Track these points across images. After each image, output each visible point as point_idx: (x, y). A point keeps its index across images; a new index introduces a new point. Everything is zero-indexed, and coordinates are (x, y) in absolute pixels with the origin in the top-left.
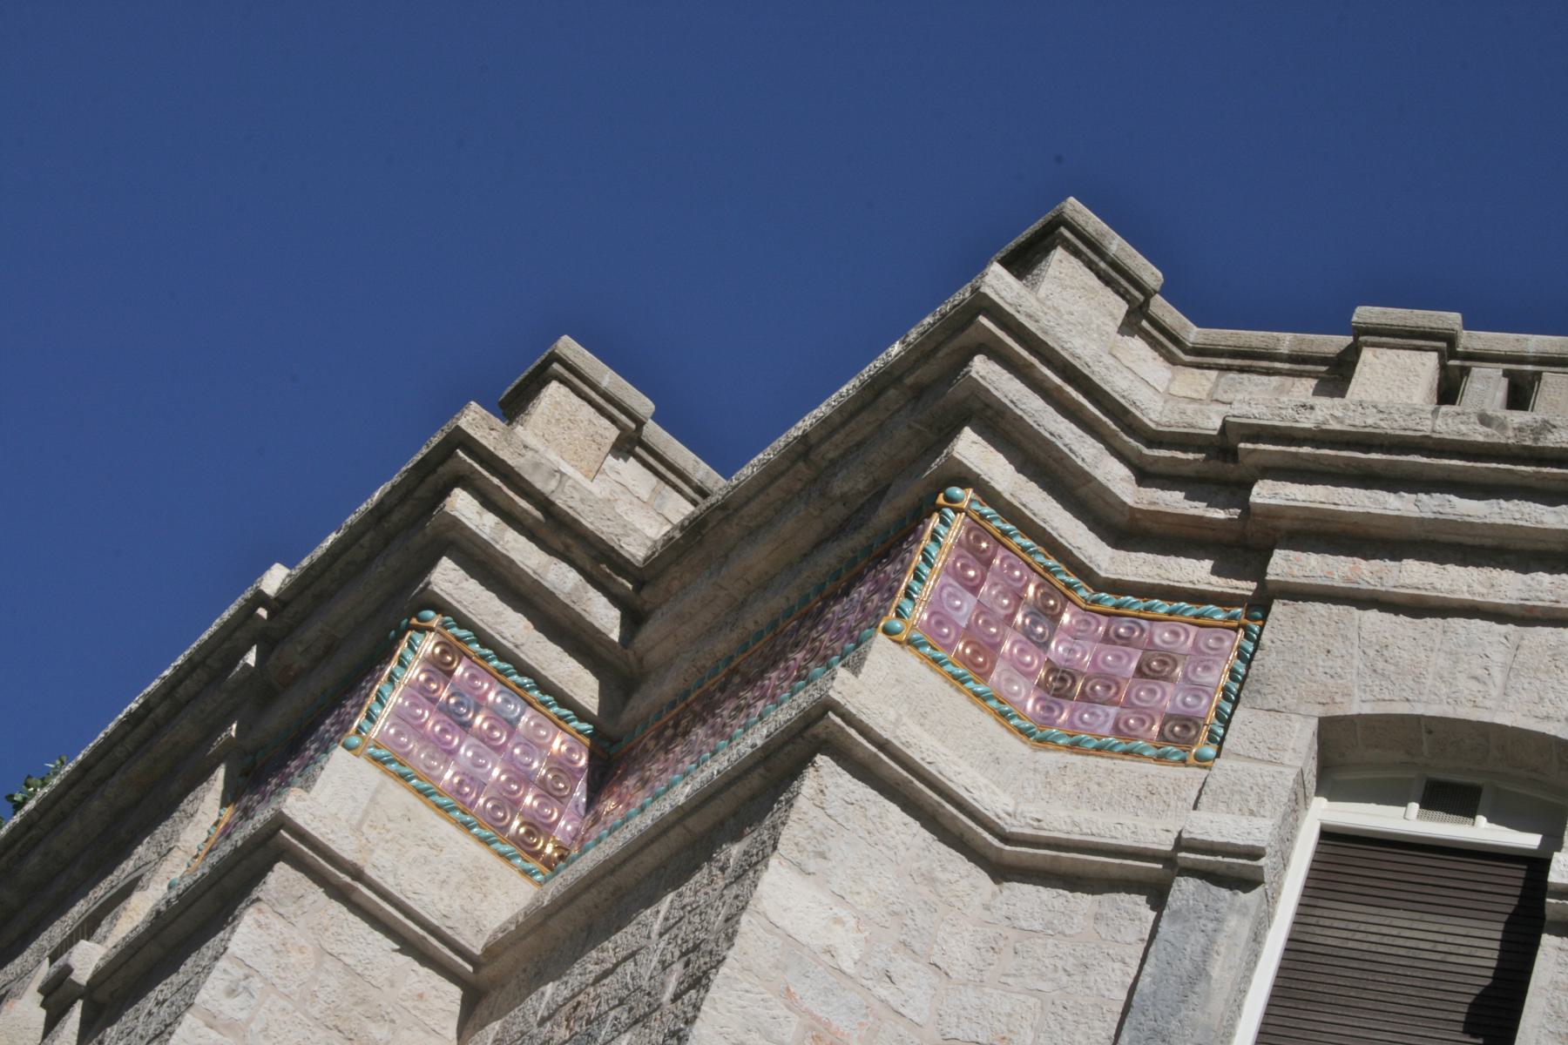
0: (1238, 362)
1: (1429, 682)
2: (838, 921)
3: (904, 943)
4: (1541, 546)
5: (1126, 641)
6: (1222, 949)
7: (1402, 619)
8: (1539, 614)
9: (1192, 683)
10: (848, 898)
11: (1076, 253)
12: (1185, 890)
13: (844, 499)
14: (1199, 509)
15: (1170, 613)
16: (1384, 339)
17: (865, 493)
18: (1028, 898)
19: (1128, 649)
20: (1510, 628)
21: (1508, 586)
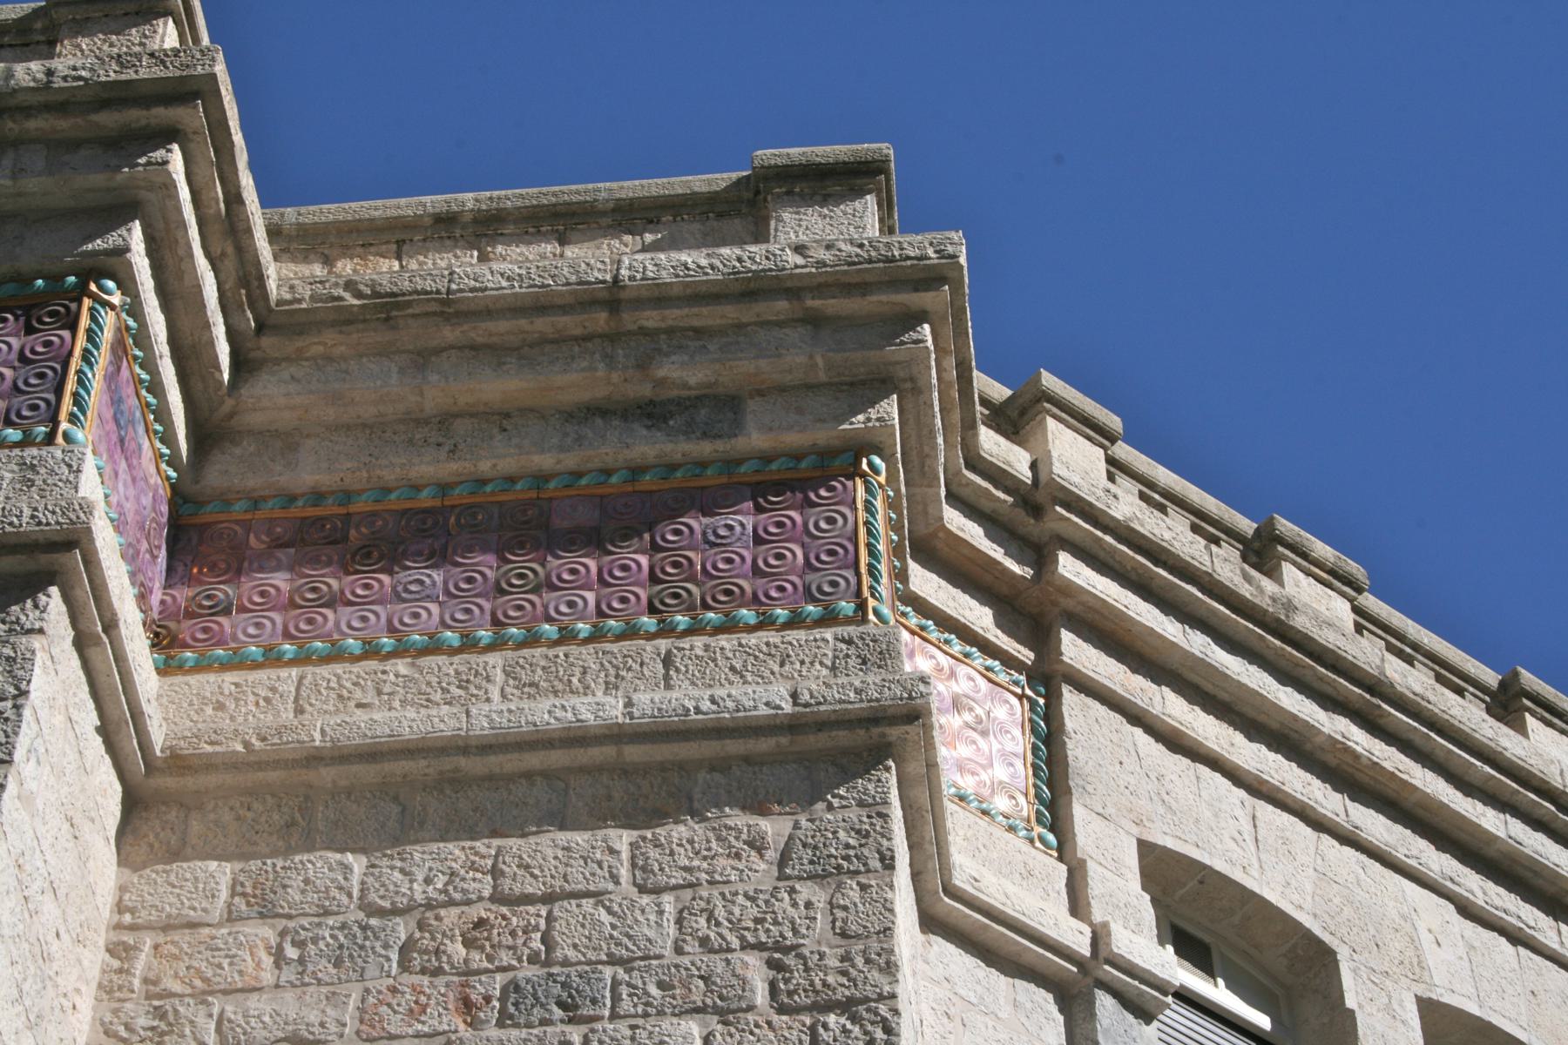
4: (1262, 718)
7: (1160, 747)
8: (1264, 789)
13: (661, 383)
14: (996, 552)
16: (1064, 415)
17: (690, 388)
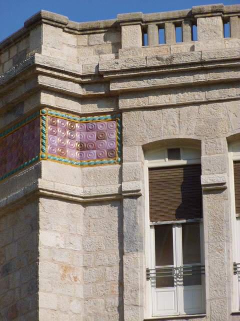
0: (92, 32)
1: (162, 129)
2: (57, 237)
3: (71, 234)
5: (92, 130)
6: (138, 215)
9: (110, 139)
10: (57, 230)
11: (47, 23)
12: (126, 201)
15: (99, 119)
18: (92, 209)
19: (93, 132)
20: (177, 109)
21: (173, 98)
